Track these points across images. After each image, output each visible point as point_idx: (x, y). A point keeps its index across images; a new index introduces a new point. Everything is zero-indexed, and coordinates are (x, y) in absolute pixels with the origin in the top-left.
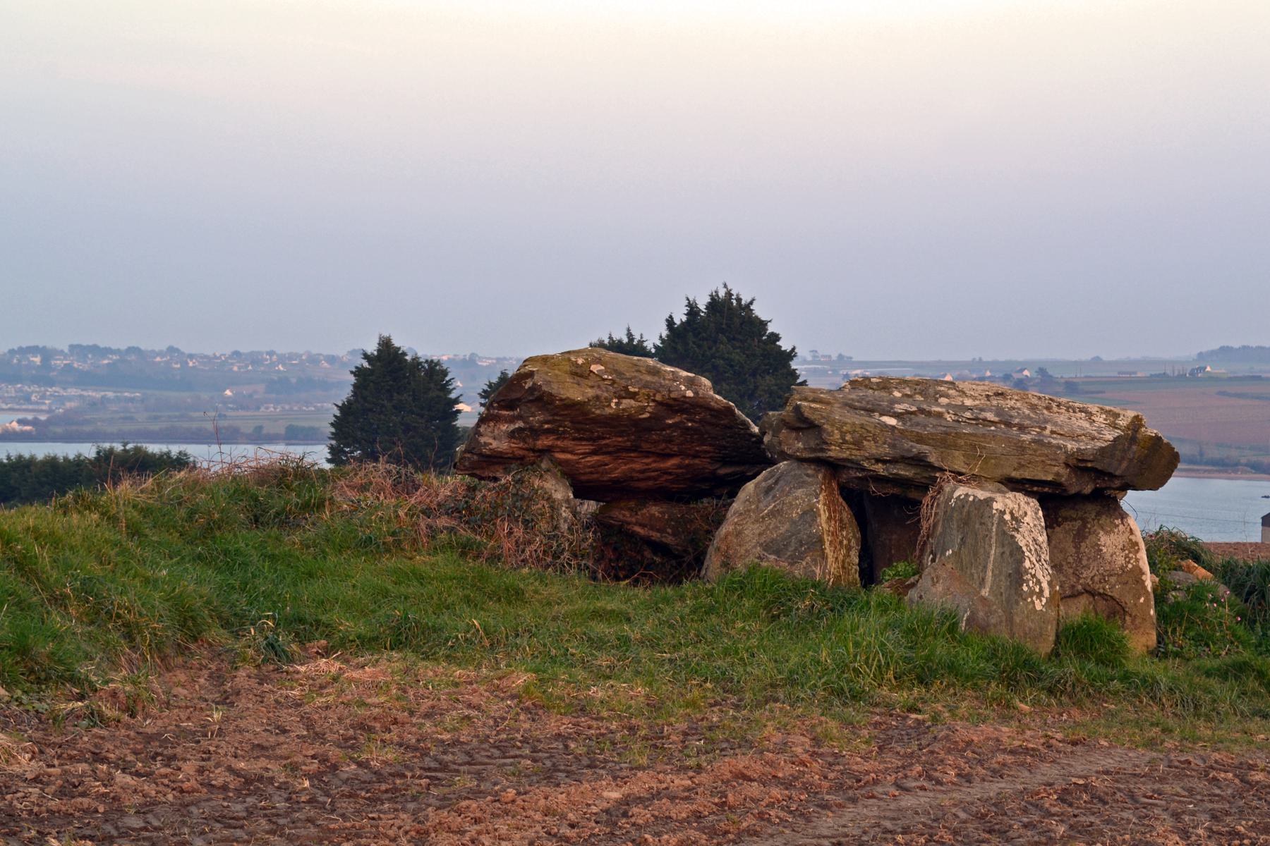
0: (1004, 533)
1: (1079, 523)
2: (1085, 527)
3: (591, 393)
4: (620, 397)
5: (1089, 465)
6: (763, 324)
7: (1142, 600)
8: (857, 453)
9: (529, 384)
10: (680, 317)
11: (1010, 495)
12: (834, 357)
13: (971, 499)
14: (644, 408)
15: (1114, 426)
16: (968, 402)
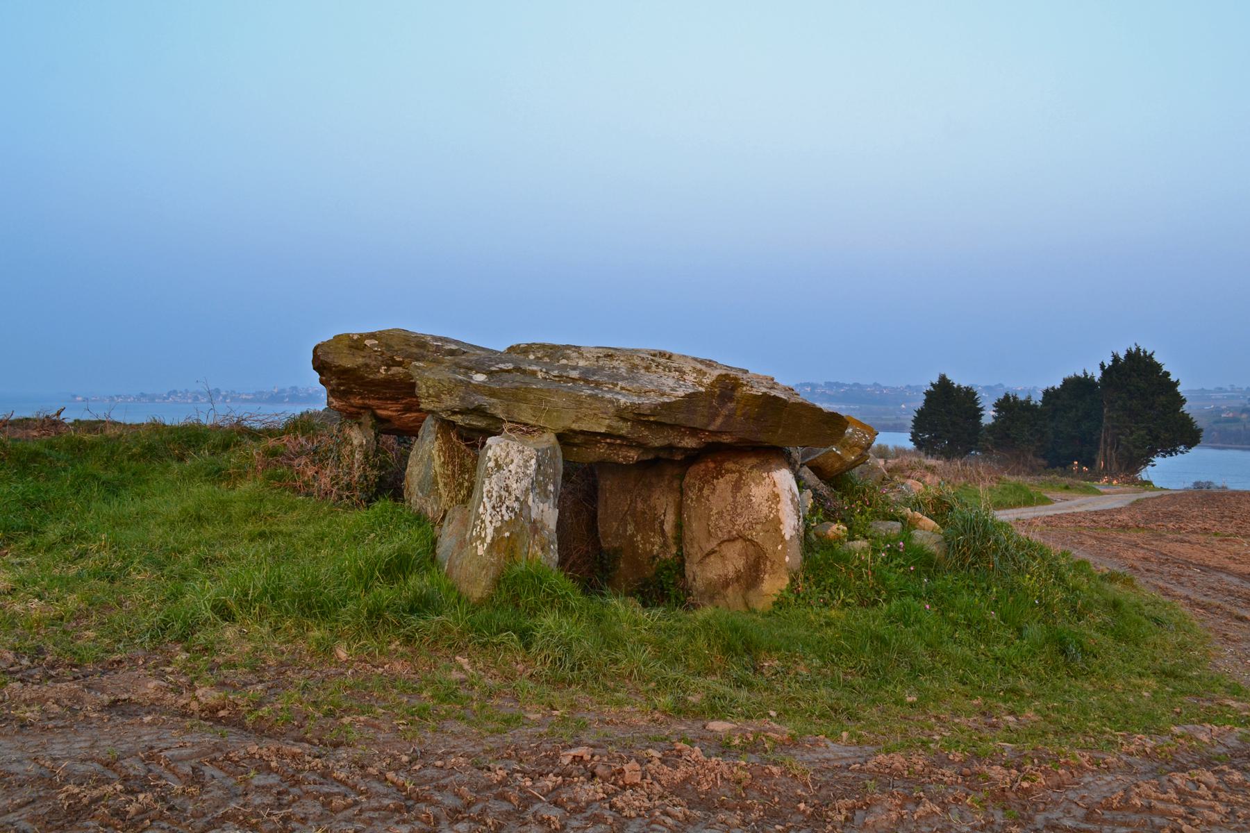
1: (737, 475)
2: (740, 478)
3: (360, 361)
5: (652, 419)
6: (1159, 367)
10: (1108, 362)
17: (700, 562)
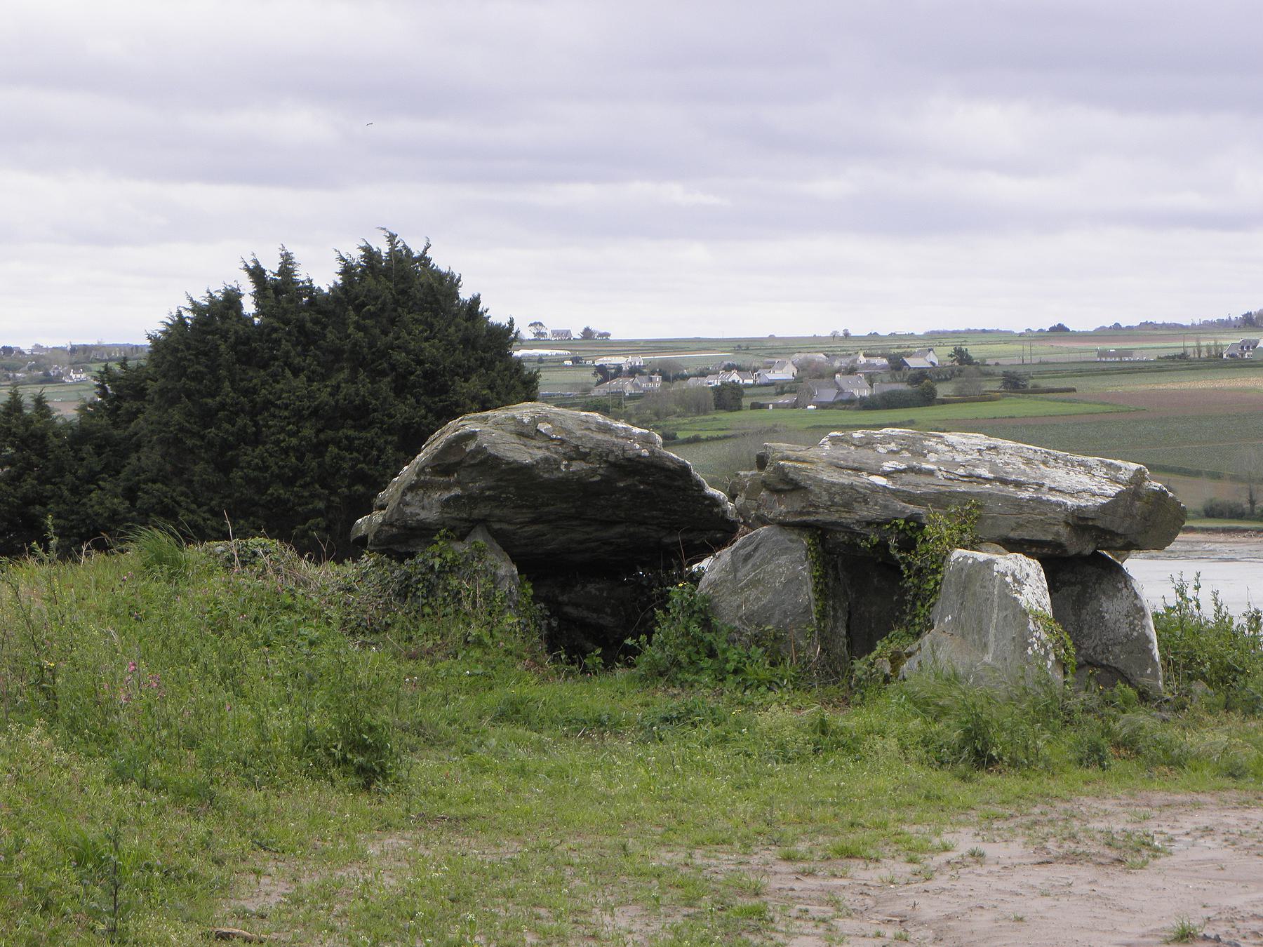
0: (1007, 596)
1: (1078, 588)
3: (540, 454)
4: (570, 459)
5: (1090, 523)
7: (1149, 671)
8: (847, 515)
9: (472, 446)
11: (1012, 555)
12: (576, 334)
13: (970, 561)
15: (1115, 481)
16: (960, 458)
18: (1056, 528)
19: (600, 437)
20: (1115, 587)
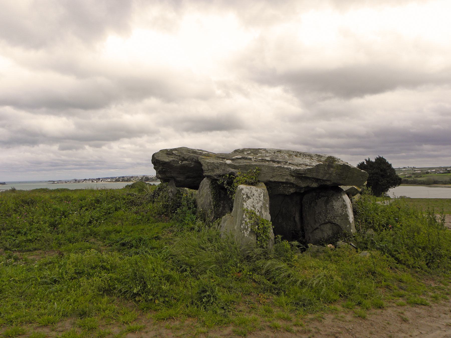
1: (326, 198)
3: (171, 159)
5: (304, 175)
7: (348, 226)
14: (191, 163)
17: (312, 232)
18: (286, 177)
19: (192, 154)
20: (337, 197)
